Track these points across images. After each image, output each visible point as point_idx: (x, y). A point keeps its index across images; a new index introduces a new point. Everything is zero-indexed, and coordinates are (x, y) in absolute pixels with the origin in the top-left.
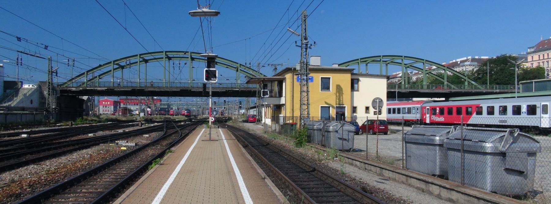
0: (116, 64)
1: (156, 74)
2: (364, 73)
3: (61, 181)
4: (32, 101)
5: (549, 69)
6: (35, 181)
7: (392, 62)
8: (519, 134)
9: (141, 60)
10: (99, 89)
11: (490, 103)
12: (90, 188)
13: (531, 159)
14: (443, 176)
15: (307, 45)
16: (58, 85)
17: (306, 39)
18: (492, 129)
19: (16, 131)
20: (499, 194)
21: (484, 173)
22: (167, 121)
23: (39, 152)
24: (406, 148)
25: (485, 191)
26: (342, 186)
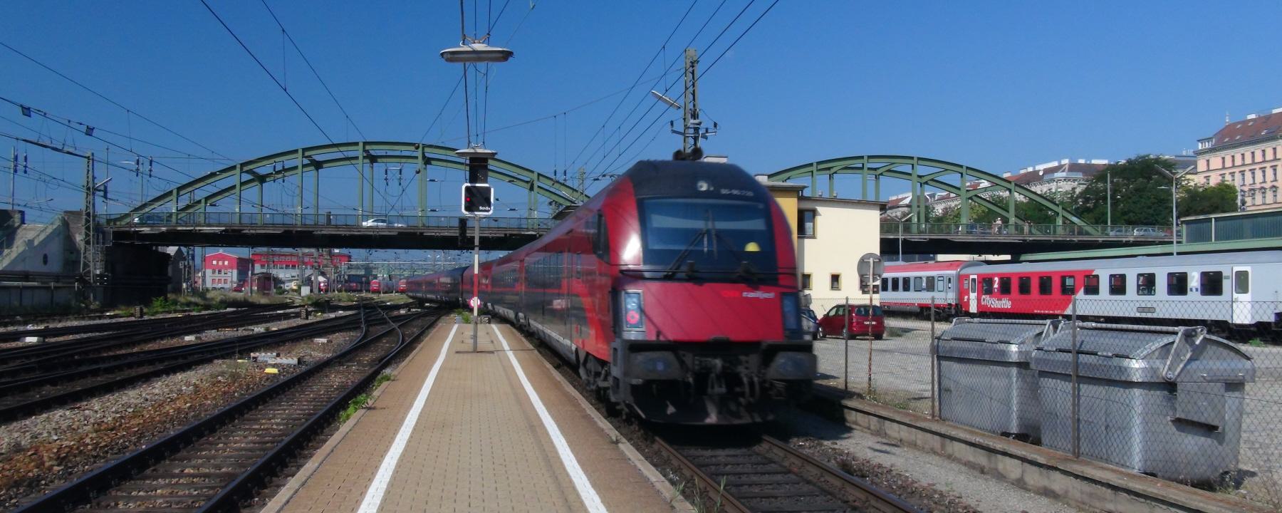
0: (247, 172)
1: (342, 196)
2: (826, 195)
3: (132, 447)
4: (45, 257)
5: (1246, 189)
6: (71, 447)
7: (889, 171)
8: (1205, 339)
9: (306, 161)
10: (206, 229)
11: (1117, 268)
12: (202, 465)
13: (1232, 398)
14: (1029, 436)
15: (697, 130)
16: (109, 221)
17: (695, 116)
18: (1119, 326)
19: (10, 329)
20: (1163, 477)
21: (1125, 429)
22: (365, 307)
23: (71, 378)
24: (939, 371)
25: (1129, 471)
26: (793, 459)
